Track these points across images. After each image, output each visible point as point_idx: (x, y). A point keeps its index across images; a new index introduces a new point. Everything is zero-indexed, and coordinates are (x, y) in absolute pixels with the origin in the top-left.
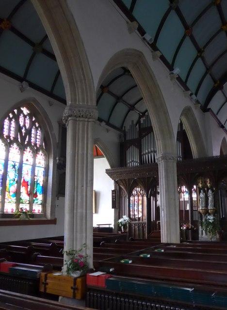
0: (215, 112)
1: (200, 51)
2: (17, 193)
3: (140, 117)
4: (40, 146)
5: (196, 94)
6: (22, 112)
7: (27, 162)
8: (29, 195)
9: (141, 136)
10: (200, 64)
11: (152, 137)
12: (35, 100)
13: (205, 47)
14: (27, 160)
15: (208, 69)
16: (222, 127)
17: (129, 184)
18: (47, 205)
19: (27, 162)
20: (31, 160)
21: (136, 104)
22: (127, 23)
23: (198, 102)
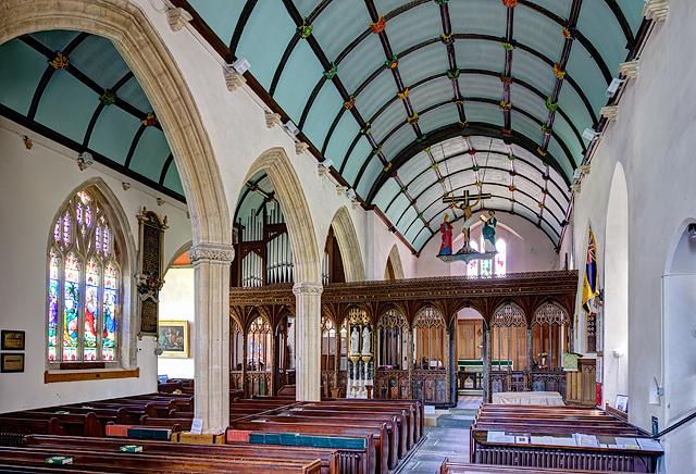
0: (383, 210)
1: (364, 126)
2: (79, 331)
3: (266, 200)
4: (109, 255)
5: (355, 188)
6: (79, 199)
7: (90, 283)
8: (95, 333)
9: (267, 239)
10: (363, 143)
11: (285, 241)
12: (101, 181)
13: (371, 121)
14: (90, 279)
15: (375, 149)
16: (393, 230)
17: (246, 314)
18: (123, 348)
19: (90, 283)
20: (96, 278)
21: (259, 180)
22: (266, 112)
23: (358, 198)
